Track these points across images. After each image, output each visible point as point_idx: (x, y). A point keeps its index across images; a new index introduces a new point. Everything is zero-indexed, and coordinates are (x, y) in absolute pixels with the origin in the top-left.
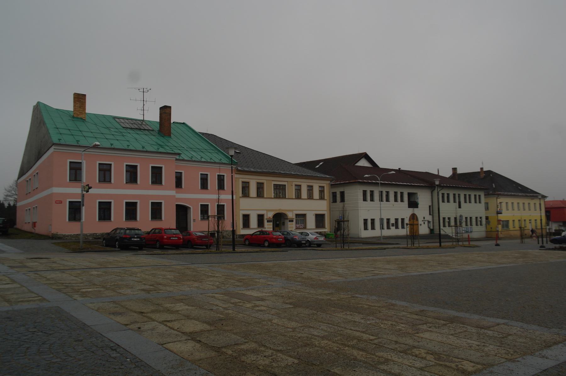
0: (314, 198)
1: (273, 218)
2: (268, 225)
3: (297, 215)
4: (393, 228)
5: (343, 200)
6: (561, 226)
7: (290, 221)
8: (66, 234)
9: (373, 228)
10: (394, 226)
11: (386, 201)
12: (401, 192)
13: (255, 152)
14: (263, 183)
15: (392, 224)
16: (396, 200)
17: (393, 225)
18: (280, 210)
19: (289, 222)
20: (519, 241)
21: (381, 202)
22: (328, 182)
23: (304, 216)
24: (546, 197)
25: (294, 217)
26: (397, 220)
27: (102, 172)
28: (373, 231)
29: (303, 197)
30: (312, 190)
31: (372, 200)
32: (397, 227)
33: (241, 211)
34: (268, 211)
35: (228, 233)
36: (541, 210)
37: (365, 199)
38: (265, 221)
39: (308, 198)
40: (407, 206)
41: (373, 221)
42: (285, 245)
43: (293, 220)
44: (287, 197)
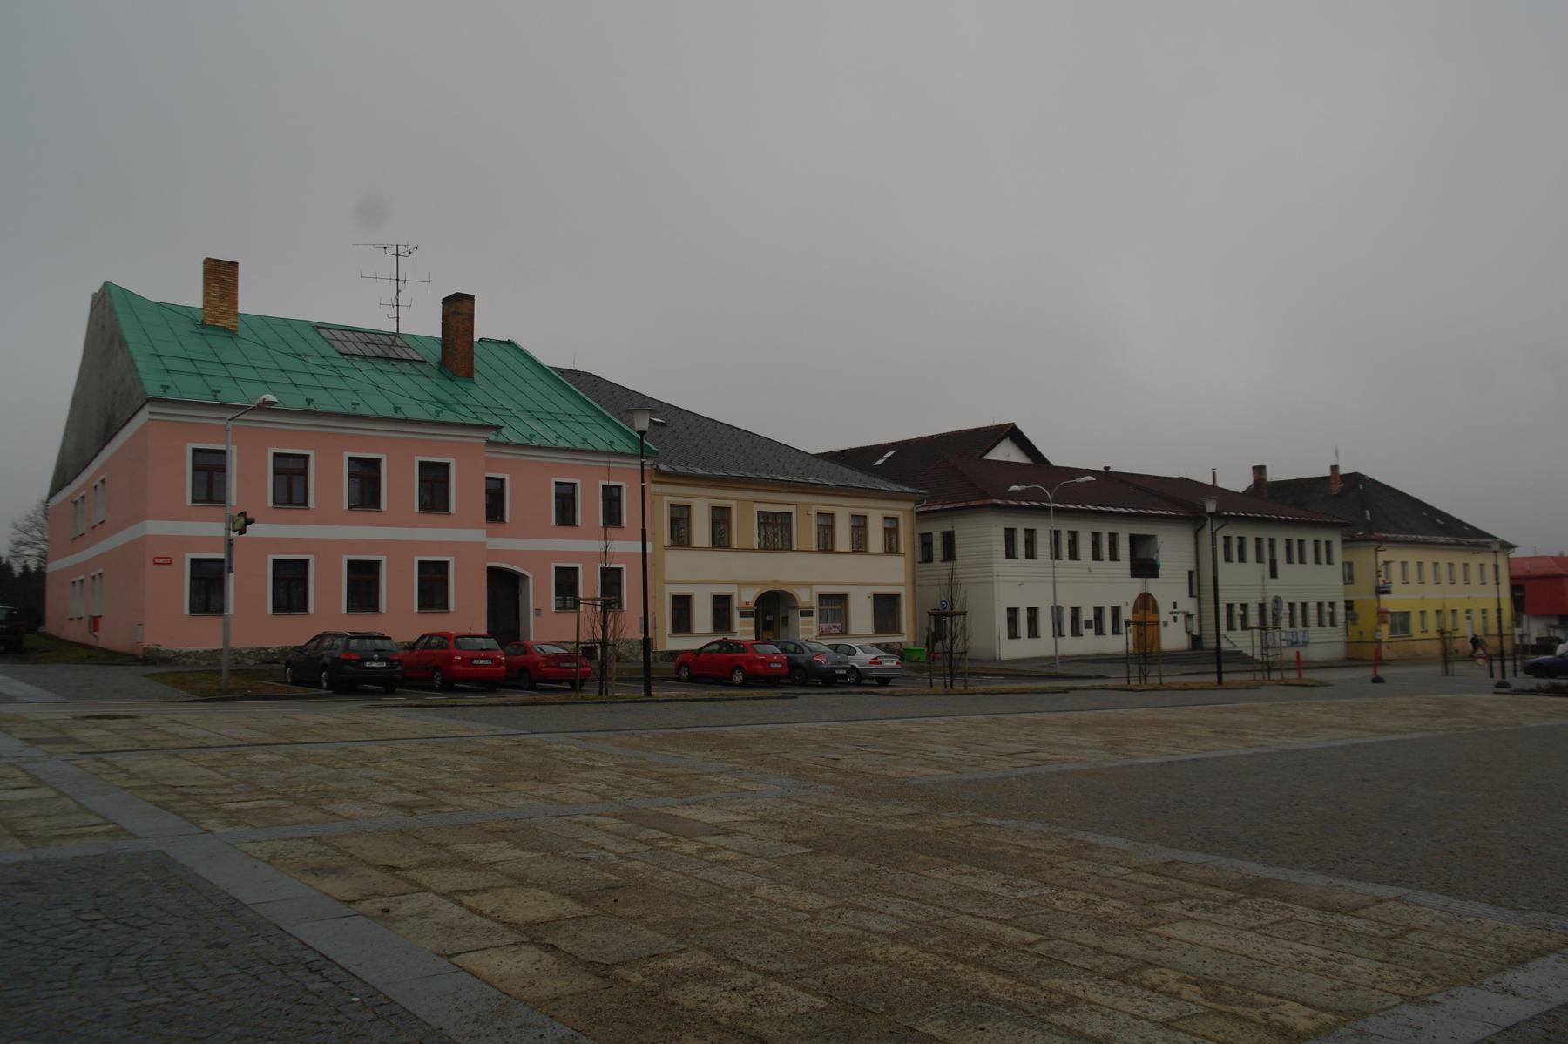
0: (871, 550)
1: (756, 604)
2: (741, 624)
3: (823, 598)
4: (1089, 634)
5: (949, 555)
6: (1554, 627)
7: (803, 614)
8: (184, 651)
9: (1033, 633)
10: (1091, 628)
11: (1070, 559)
12: (1110, 534)
13: (707, 422)
14: (729, 508)
15: (1085, 621)
16: (1097, 556)
17: (1088, 624)
18: (775, 582)
19: (801, 616)
20: (1438, 669)
21: (1056, 562)
22: (910, 506)
23: (842, 599)
24: (1513, 547)
25: (815, 602)
26: (1099, 611)
27: (284, 478)
28: (1034, 641)
31: (1031, 554)
32: (1099, 631)
33: (666, 586)
34: (741, 585)
35: (631, 647)
37: (1010, 554)
38: (735, 614)
39: (854, 551)
40: (1129, 572)
41: (1033, 613)
42: (789, 681)
43: (812, 612)
44: (795, 548)
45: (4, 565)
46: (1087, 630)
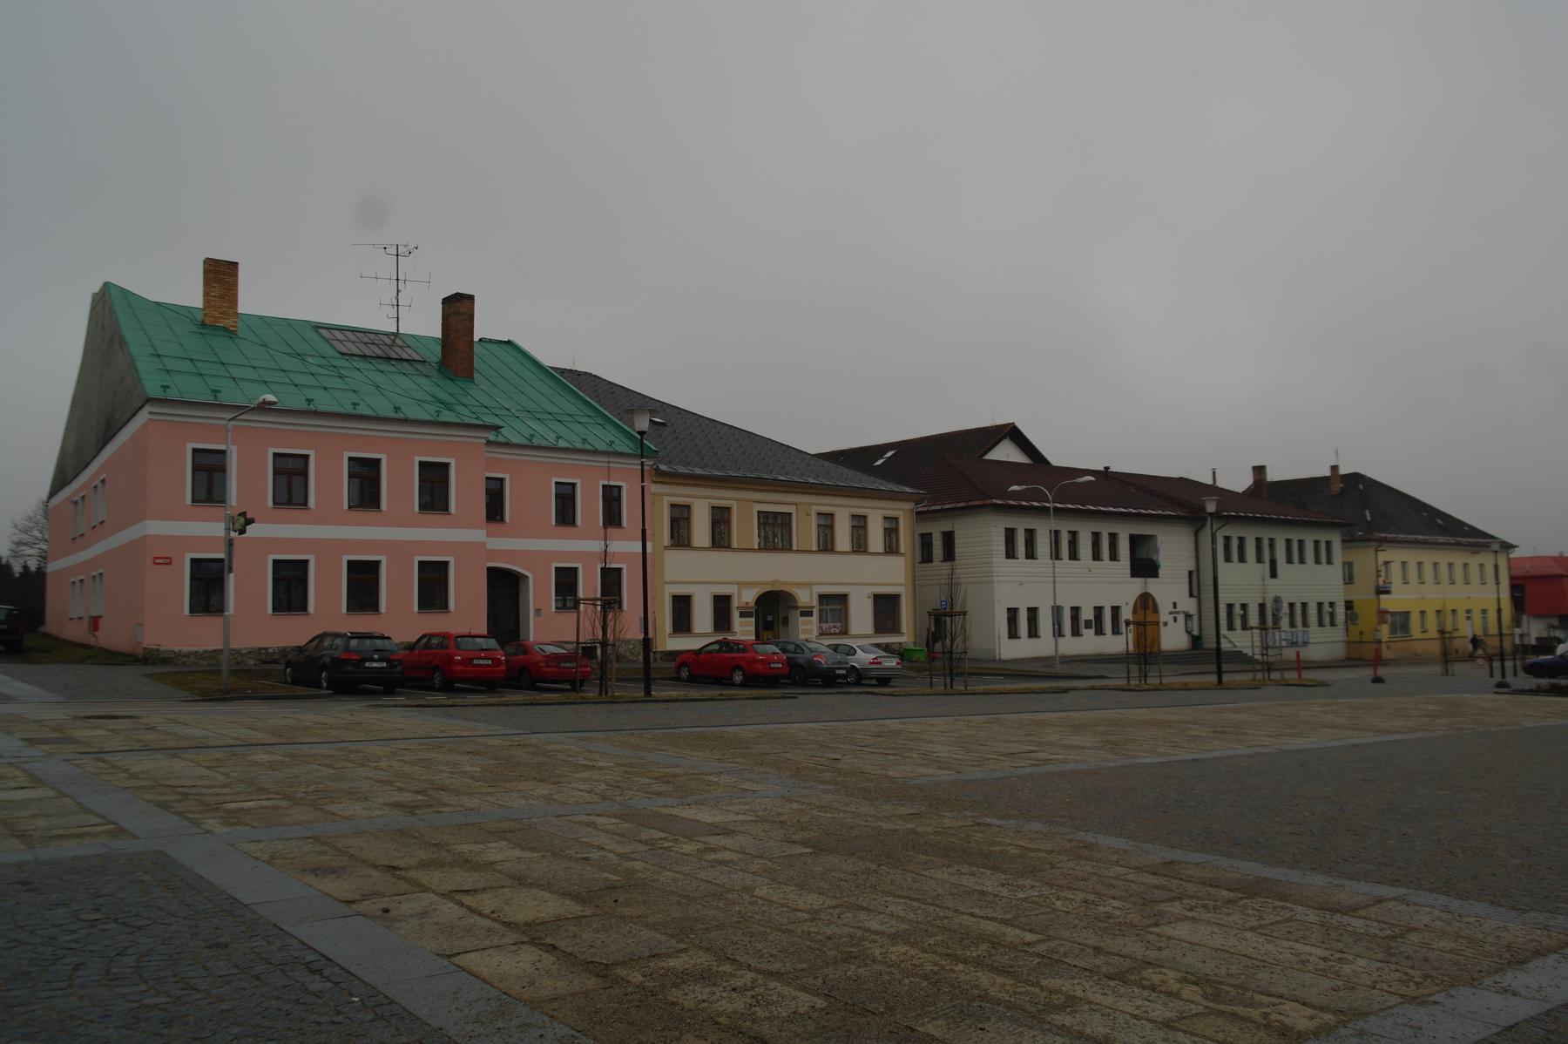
0: (871, 550)
1: (756, 604)
2: (741, 624)
3: (823, 598)
4: (1089, 634)
5: (949, 555)
6: (1554, 627)
7: (803, 614)
8: (184, 651)
9: (1033, 633)
10: (1091, 628)
11: (1070, 559)
12: (1110, 534)
14: (729, 508)
15: (1085, 621)
16: (1097, 556)
17: (1088, 624)
18: (775, 582)
19: (801, 616)
21: (1056, 562)
22: (910, 506)
23: (842, 599)
25: (815, 602)
26: (1099, 611)
28: (1034, 641)
29: (839, 547)
30: (865, 527)
31: (1031, 554)
32: (1099, 631)
33: (666, 586)
34: (741, 585)
35: (631, 647)
36: (1498, 584)
37: (1010, 554)
38: (735, 614)
39: (854, 551)
40: (1129, 572)
41: (1033, 613)
42: (789, 681)
43: (812, 612)
44: (795, 548)
45: (4, 565)
46: (1087, 630)
